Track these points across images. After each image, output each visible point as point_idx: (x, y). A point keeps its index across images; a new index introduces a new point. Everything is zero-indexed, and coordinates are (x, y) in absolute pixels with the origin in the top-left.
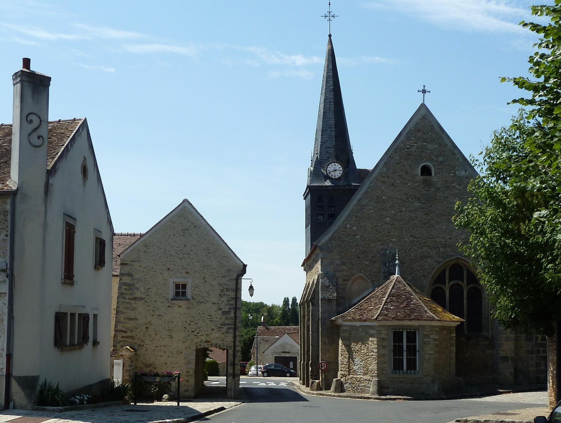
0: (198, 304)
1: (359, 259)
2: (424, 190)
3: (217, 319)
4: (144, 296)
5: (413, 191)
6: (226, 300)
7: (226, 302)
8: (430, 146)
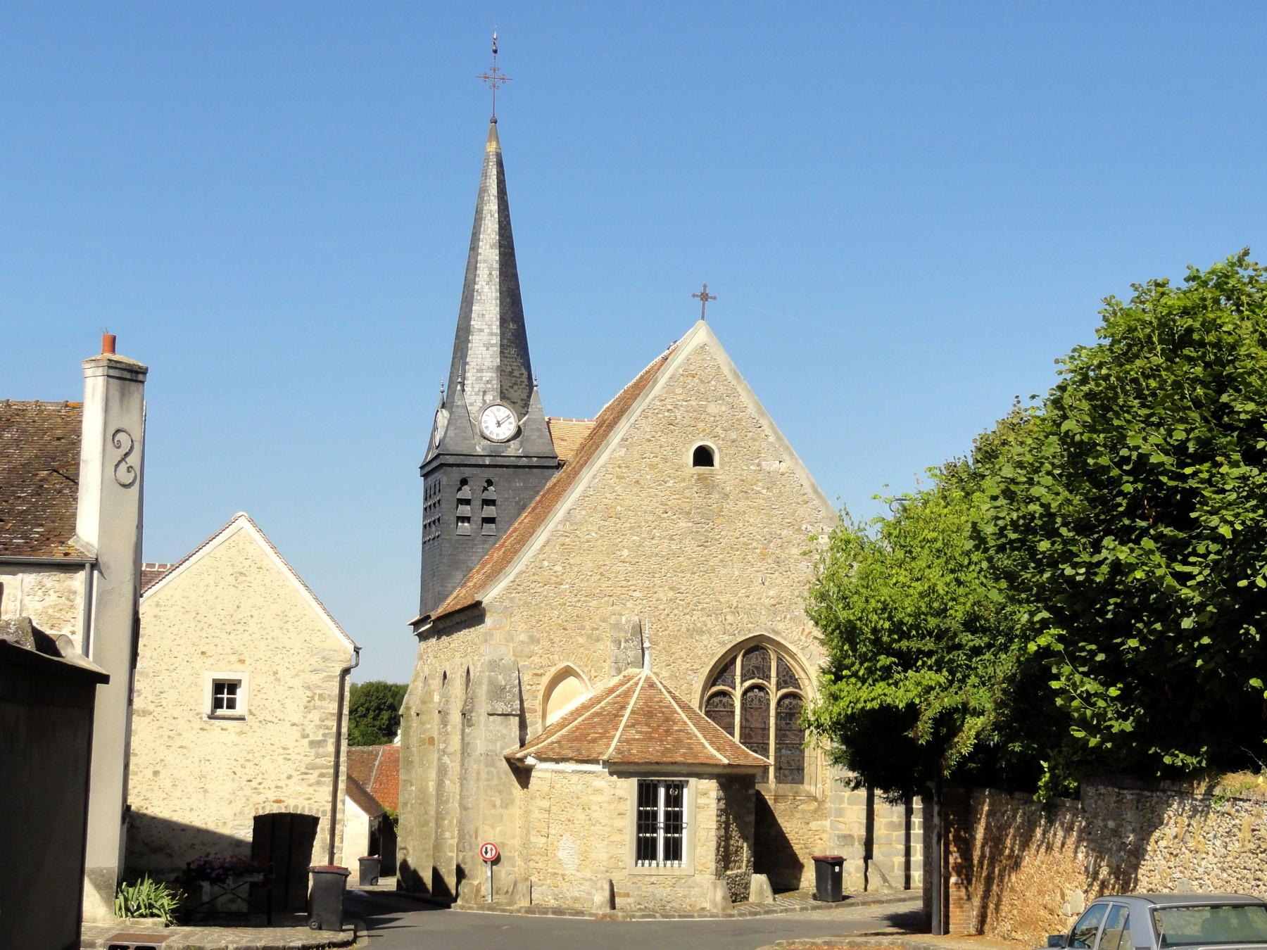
2: (699, 497)
3: (299, 757)
4: (151, 708)
5: (677, 496)
7: (317, 722)
8: (713, 408)
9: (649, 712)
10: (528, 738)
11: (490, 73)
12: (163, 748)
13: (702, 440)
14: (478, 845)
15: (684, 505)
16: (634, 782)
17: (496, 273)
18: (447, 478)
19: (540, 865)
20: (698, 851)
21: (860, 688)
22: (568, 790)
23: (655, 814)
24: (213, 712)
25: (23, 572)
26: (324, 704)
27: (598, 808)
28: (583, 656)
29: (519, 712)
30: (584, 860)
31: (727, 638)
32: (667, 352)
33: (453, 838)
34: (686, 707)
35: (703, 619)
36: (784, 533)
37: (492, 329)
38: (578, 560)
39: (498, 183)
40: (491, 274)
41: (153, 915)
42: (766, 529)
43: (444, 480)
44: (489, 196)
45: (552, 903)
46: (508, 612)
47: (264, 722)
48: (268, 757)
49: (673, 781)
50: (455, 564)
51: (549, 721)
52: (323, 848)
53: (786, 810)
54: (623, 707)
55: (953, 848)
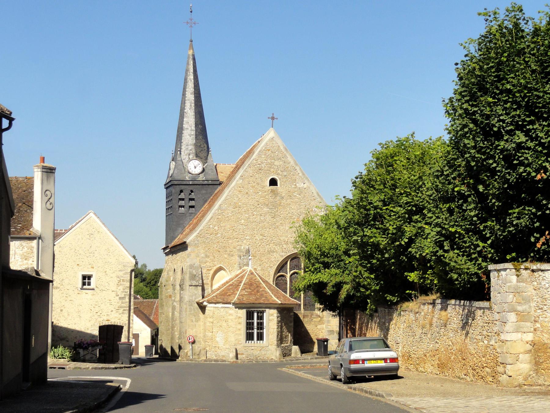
4: (59, 286)
8: (277, 163)
9: (251, 284)
10: (206, 295)
11: (189, 21)
12: (64, 301)
17: (193, 105)
19: (210, 344)
21: (312, 276)
23: (253, 323)
24: (82, 287)
25: (15, 241)
26: (124, 283)
32: (261, 138)
34: (265, 282)
41: (63, 358)
43: (173, 191)
45: (215, 358)
46: (196, 246)
51: (213, 288)
53: (308, 321)
54: (241, 282)
55: (349, 332)
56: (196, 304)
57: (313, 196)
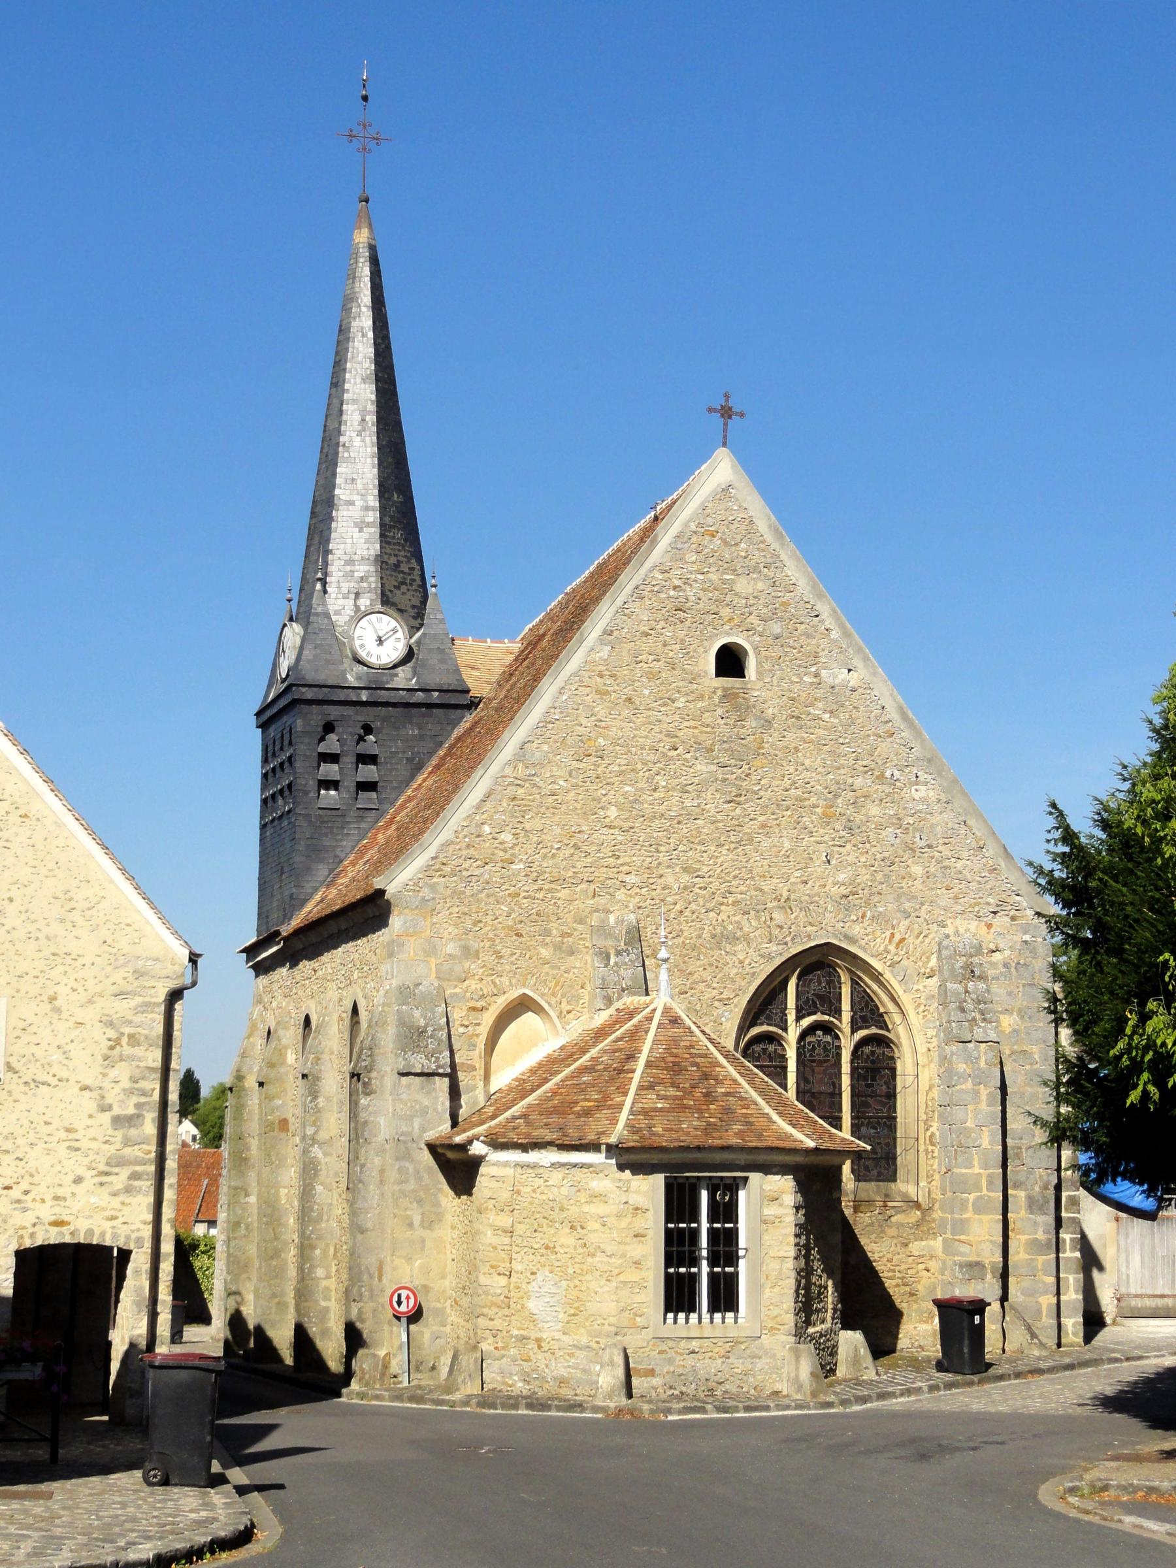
0: (27, 1089)
1: (520, 940)
2: (726, 724)
3: (95, 1145)
5: (692, 723)
6: (128, 1075)
7: (126, 1083)
8: (743, 585)
9: (675, 1064)
10: (463, 1112)
13: (728, 635)
14: (382, 1291)
15: (703, 737)
16: (659, 1180)
17: (371, 419)
18: (303, 723)
19: (497, 1323)
20: (766, 1296)
22: (544, 1197)
23: (694, 1234)
26: (138, 1051)
27: (597, 1226)
28: (549, 978)
29: (449, 1070)
30: (574, 1315)
31: (774, 948)
33: (328, 1277)
35: (737, 918)
36: (858, 782)
37: (366, 501)
38: (537, 824)
39: (371, 288)
40: (363, 420)
42: (831, 776)
43: (299, 725)
44: (359, 306)
45: (520, 1387)
46: (427, 908)
47: (32, 1085)
48: (41, 1145)
49: (722, 1178)
50: (316, 852)
51: (493, 1088)
52: (137, 1304)
54: (631, 1057)
56: (426, 1153)
57: (884, 719)
